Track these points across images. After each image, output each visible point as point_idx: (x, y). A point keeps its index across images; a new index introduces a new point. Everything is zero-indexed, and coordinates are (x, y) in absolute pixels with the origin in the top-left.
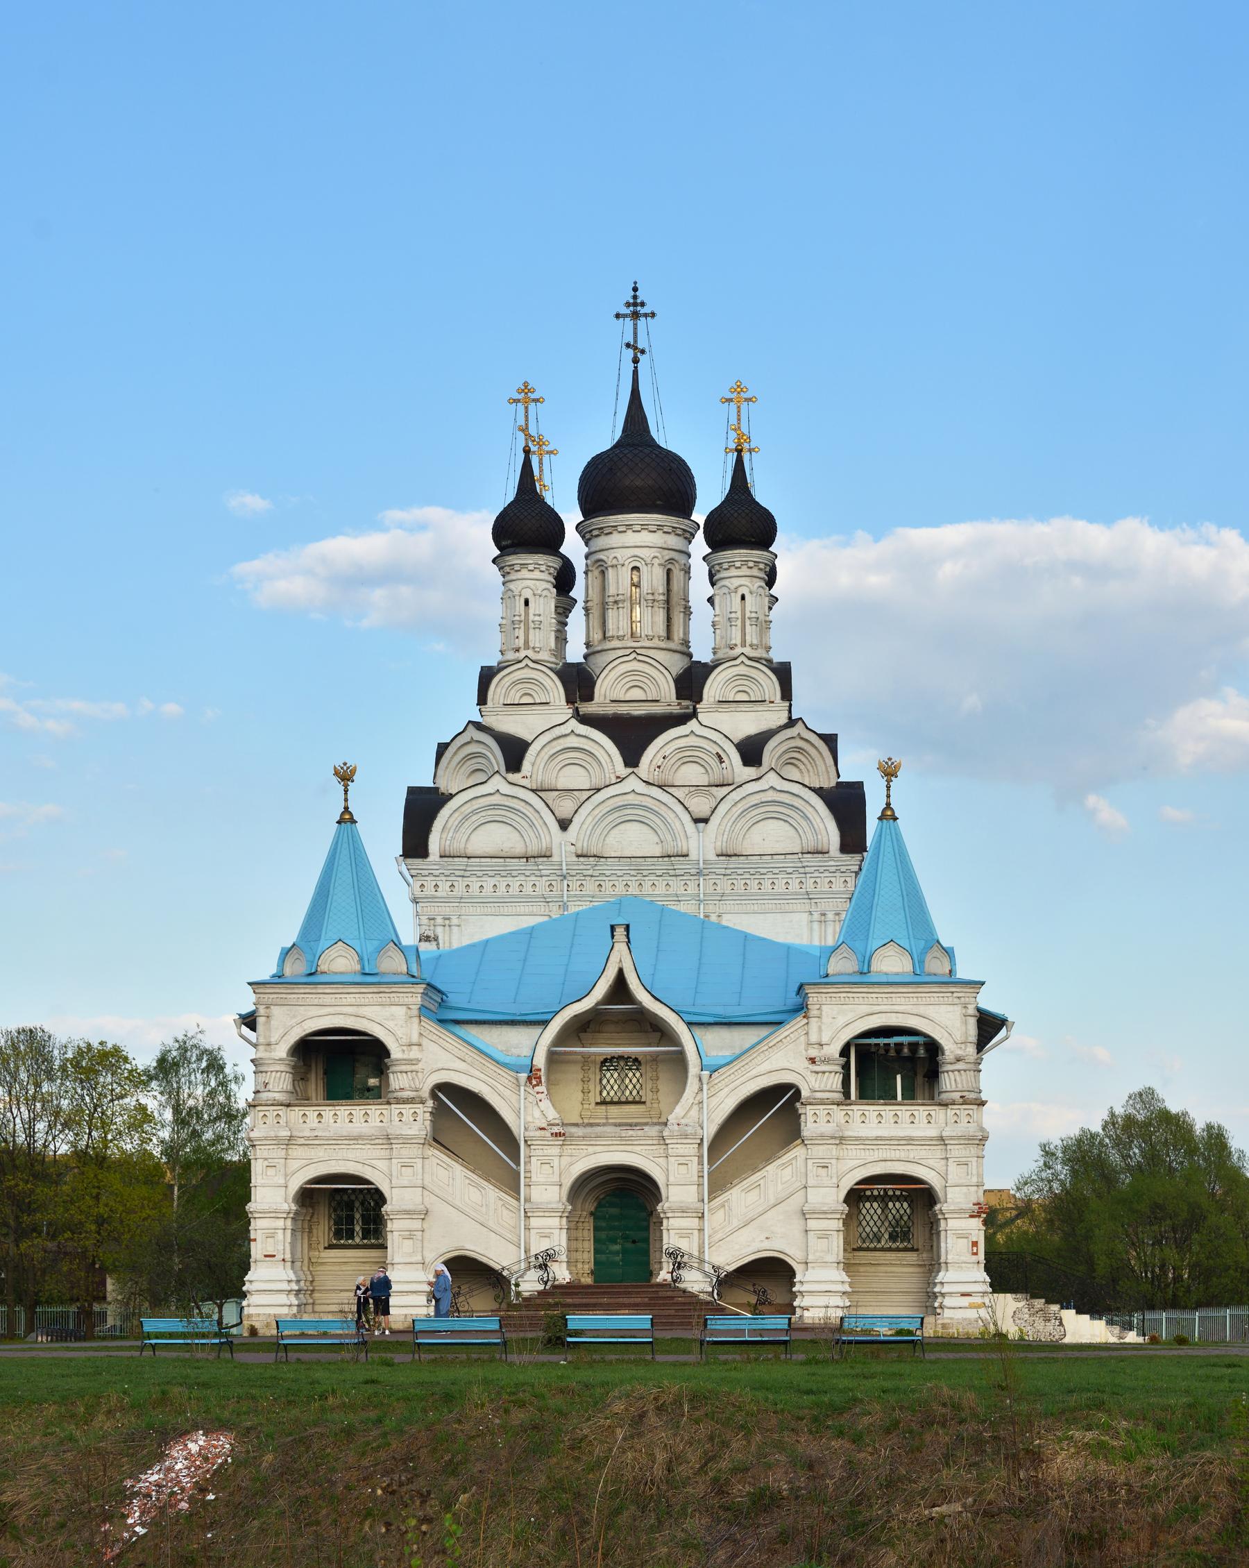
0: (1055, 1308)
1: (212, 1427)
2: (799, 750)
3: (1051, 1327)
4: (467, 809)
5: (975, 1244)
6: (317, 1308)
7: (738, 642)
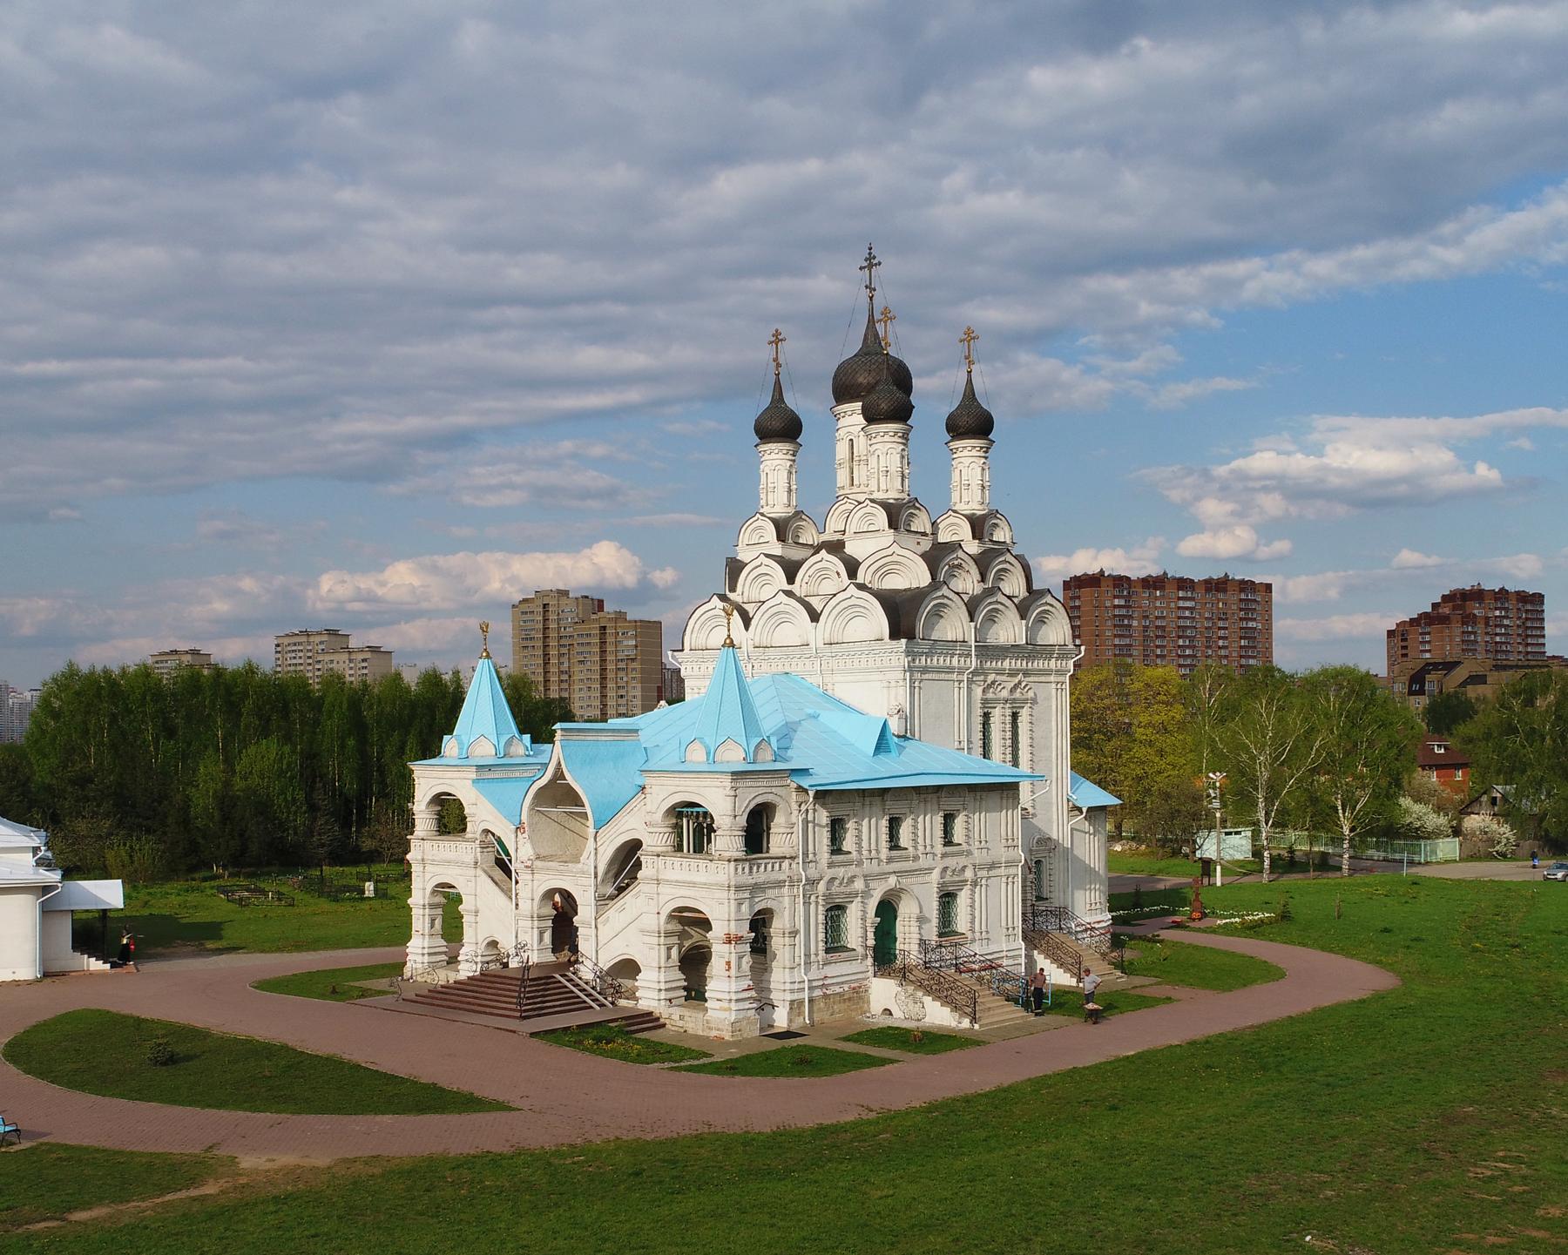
0: (920, 994)
1: (625, 539)
4: (835, 612)
5: (728, 963)
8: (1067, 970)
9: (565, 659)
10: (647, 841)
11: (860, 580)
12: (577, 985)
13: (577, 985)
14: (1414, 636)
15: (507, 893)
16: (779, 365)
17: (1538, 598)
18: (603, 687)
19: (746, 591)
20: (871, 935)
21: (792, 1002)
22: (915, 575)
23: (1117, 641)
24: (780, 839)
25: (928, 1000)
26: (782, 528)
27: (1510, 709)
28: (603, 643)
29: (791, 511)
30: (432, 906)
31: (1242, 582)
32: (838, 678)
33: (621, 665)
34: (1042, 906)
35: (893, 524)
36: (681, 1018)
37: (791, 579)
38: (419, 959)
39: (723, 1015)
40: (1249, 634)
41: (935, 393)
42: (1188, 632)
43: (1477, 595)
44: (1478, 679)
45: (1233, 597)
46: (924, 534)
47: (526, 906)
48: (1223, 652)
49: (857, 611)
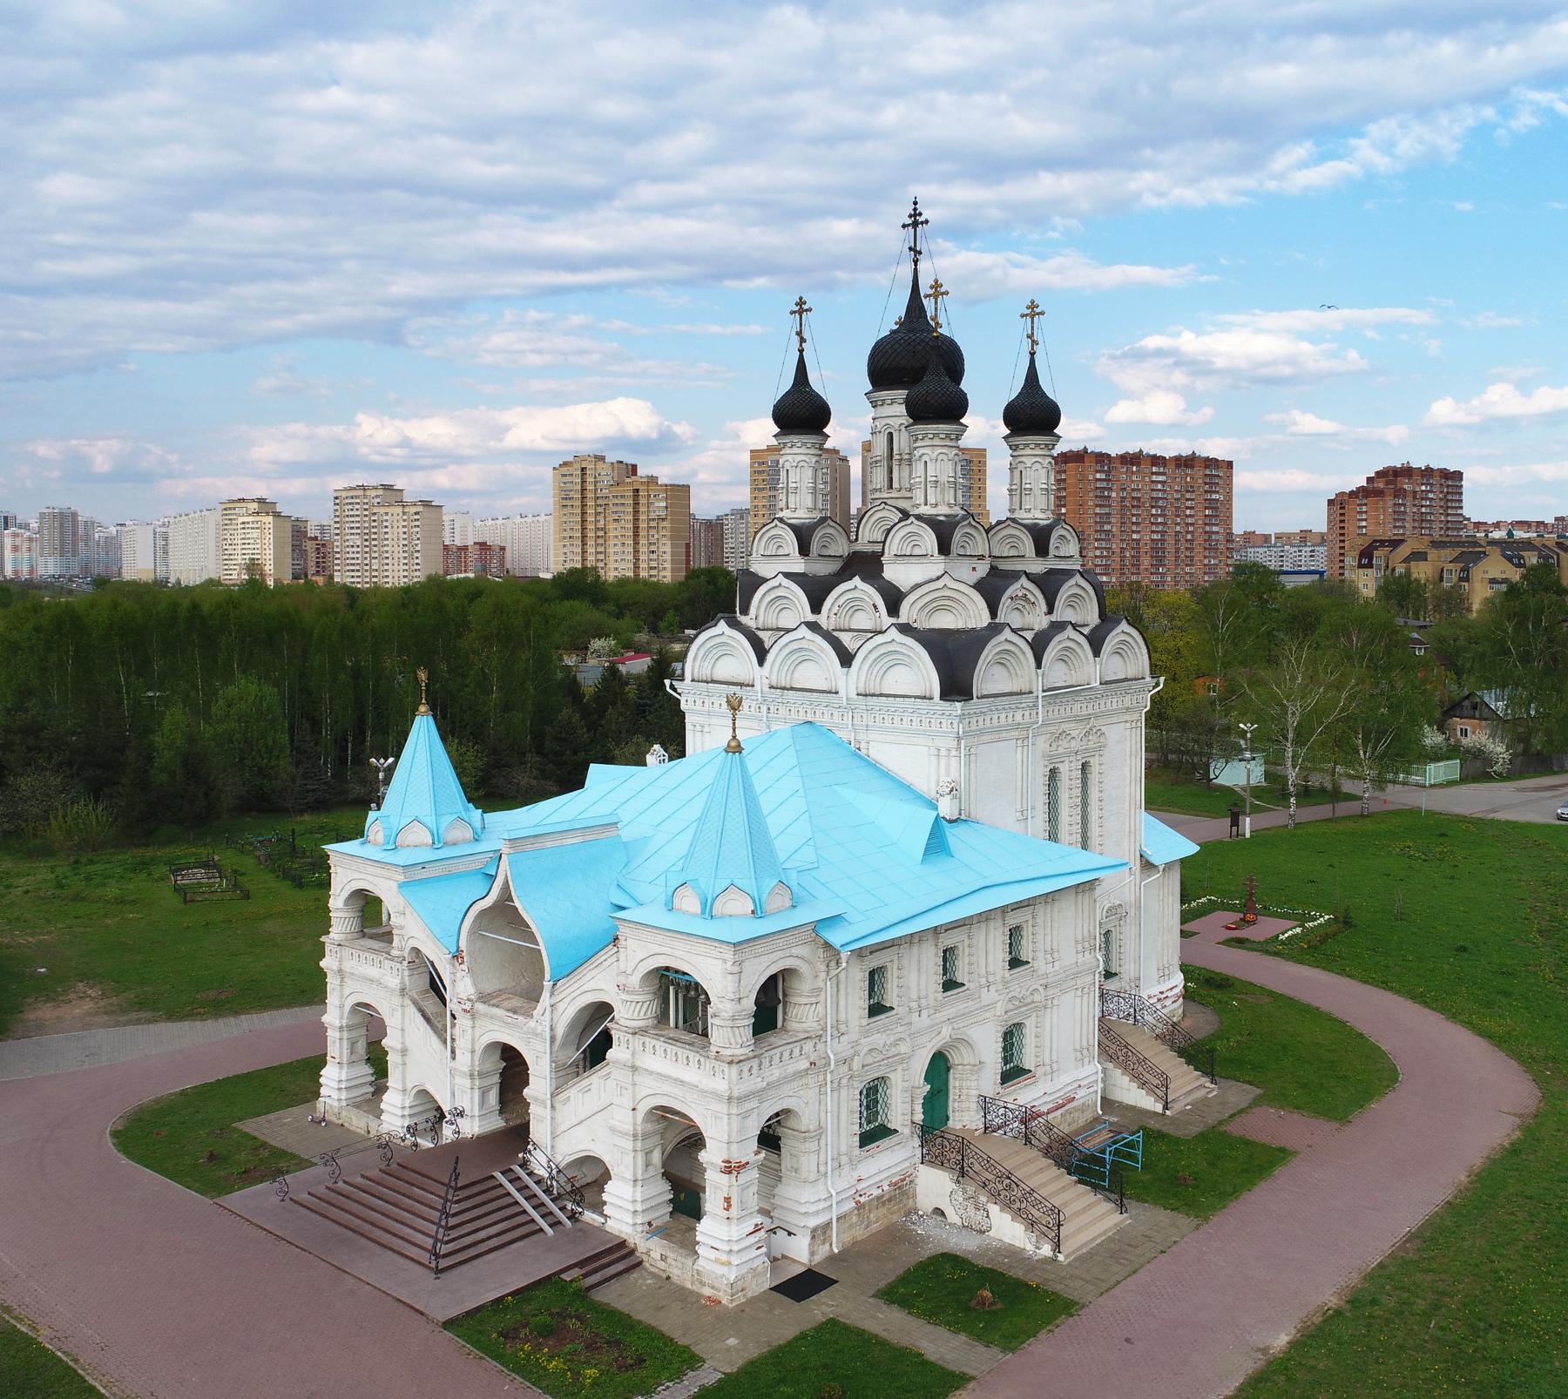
2: (1067, 648)
3: (980, 1215)
4: (709, 644)
5: (728, 1200)
6: (923, 993)
7: (922, 501)
8: (1151, 1092)
9: (601, 518)
10: (620, 1012)
11: (903, 619)
12: (523, 1188)
13: (523, 1188)
14: (1352, 506)
15: (440, 1033)
16: (802, 340)
17: (1458, 475)
18: (636, 543)
19: (759, 612)
20: (919, 1109)
21: (814, 1230)
22: (975, 614)
23: (1098, 510)
24: (802, 1014)
25: (994, 1209)
26: (804, 536)
27: (1505, 631)
28: (636, 504)
29: (817, 515)
30: (350, 1028)
31: (1207, 459)
32: (872, 736)
33: (653, 524)
34: (1112, 985)
35: (944, 548)
36: (663, 1258)
37: (816, 607)
38: (335, 1095)
39: (720, 1270)
40: (1212, 504)
41: (988, 388)
42: (1160, 503)
43: (1406, 472)
44: (1419, 556)
45: (1199, 472)
46: (981, 557)
47: (464, 1061)
48: (1190, 520)
49: (893, 660)
